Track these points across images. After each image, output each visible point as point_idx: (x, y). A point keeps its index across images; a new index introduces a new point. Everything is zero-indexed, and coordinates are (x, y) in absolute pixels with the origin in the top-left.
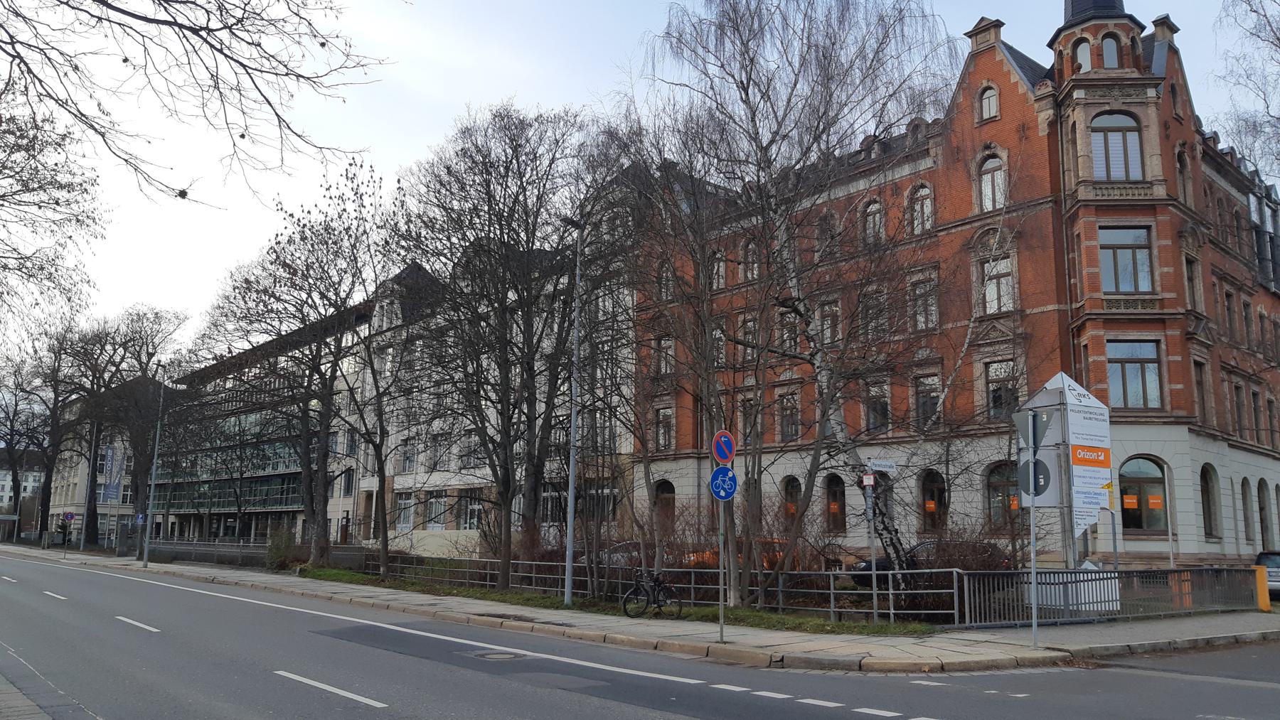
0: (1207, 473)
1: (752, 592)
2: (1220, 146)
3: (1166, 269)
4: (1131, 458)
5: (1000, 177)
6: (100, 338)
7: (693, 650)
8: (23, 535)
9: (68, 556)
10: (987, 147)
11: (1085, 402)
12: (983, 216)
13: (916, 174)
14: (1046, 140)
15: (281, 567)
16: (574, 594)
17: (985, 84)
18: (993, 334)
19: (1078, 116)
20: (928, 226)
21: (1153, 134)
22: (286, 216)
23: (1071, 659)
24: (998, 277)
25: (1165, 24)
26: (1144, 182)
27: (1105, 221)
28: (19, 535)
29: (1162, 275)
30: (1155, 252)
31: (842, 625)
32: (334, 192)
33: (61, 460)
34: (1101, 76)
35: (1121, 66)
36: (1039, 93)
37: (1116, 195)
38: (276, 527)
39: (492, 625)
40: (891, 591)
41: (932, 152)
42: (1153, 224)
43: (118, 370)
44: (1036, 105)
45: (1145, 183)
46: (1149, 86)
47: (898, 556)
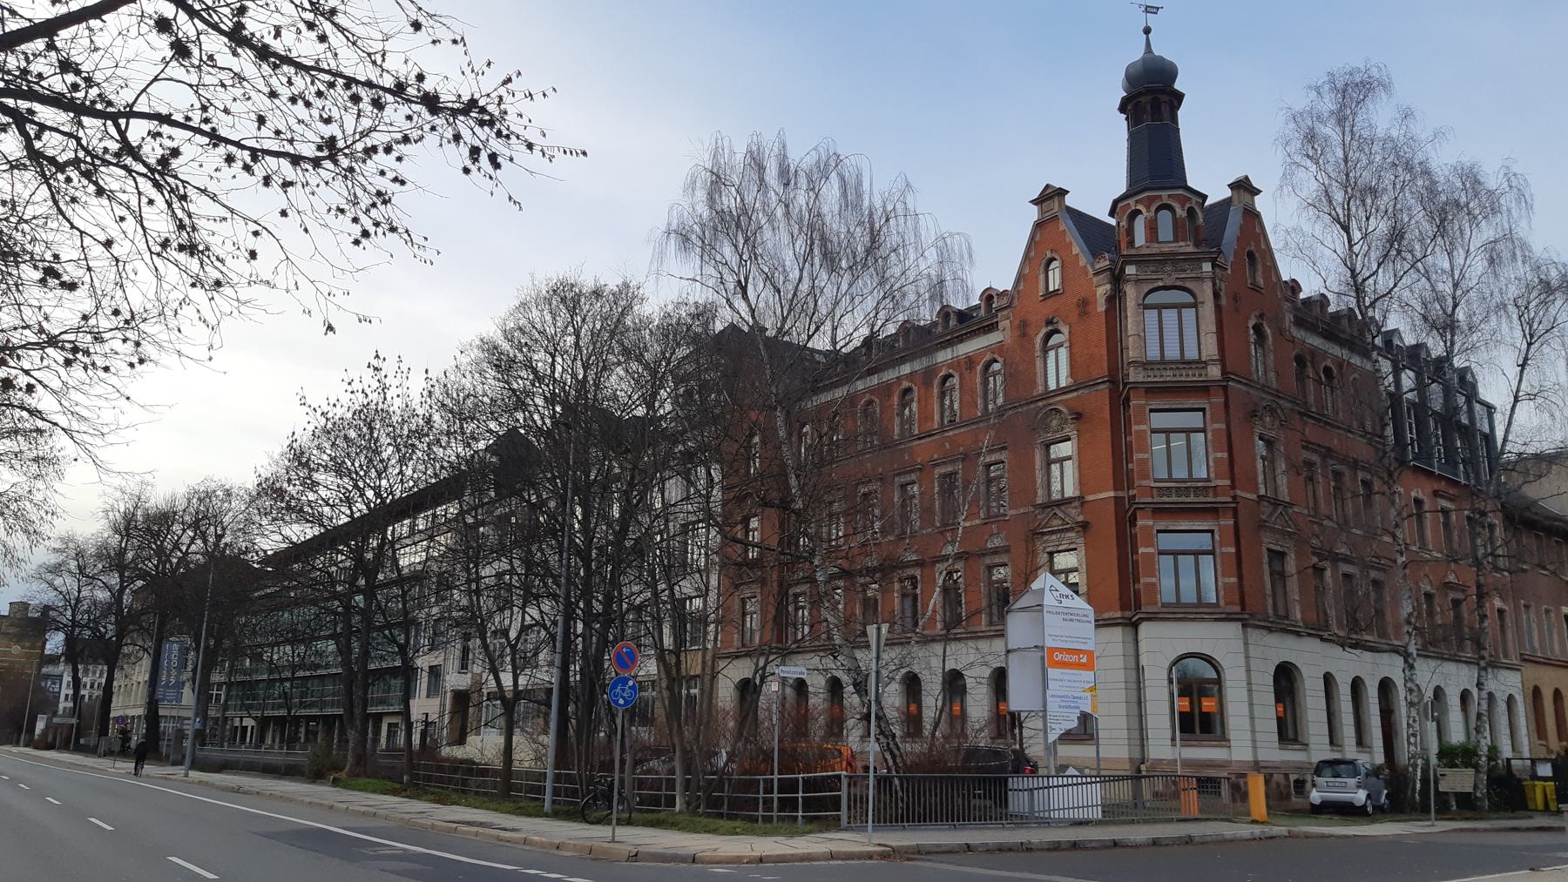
0: (1286, 678)
2: (1332, 309)
3: (1219, 455)
4: (1174, 663)
5: (1063, 352)
6: (164, 519)
8: (82, 741)
9: (119, 764)
10: (1049, 322)
12: (1048, 395)
15: (317, 776)
16: (554, 802)
17: (1049, 255)
18: (1056, 522)
19: (1131, 293)
20: (1000, 401)
21: (1208, 310)
24: (1061, 461)
25: (1243, 187)
26: (1199, 362)
27: (1155, 404)
28: (77, 741)
29: (1216, 460)
30: (1209, 436)
31: (790, 828)
32: (356, 386)
33: (125, 655)
34: (1154, 251)
35: (1176, 240)
37: (1168, 376)
39: (449, 830)
40: (762, 795)
41: (1001, 325)
42: (1207, 406)
45: (1200, 364)
46: (1205, 260)
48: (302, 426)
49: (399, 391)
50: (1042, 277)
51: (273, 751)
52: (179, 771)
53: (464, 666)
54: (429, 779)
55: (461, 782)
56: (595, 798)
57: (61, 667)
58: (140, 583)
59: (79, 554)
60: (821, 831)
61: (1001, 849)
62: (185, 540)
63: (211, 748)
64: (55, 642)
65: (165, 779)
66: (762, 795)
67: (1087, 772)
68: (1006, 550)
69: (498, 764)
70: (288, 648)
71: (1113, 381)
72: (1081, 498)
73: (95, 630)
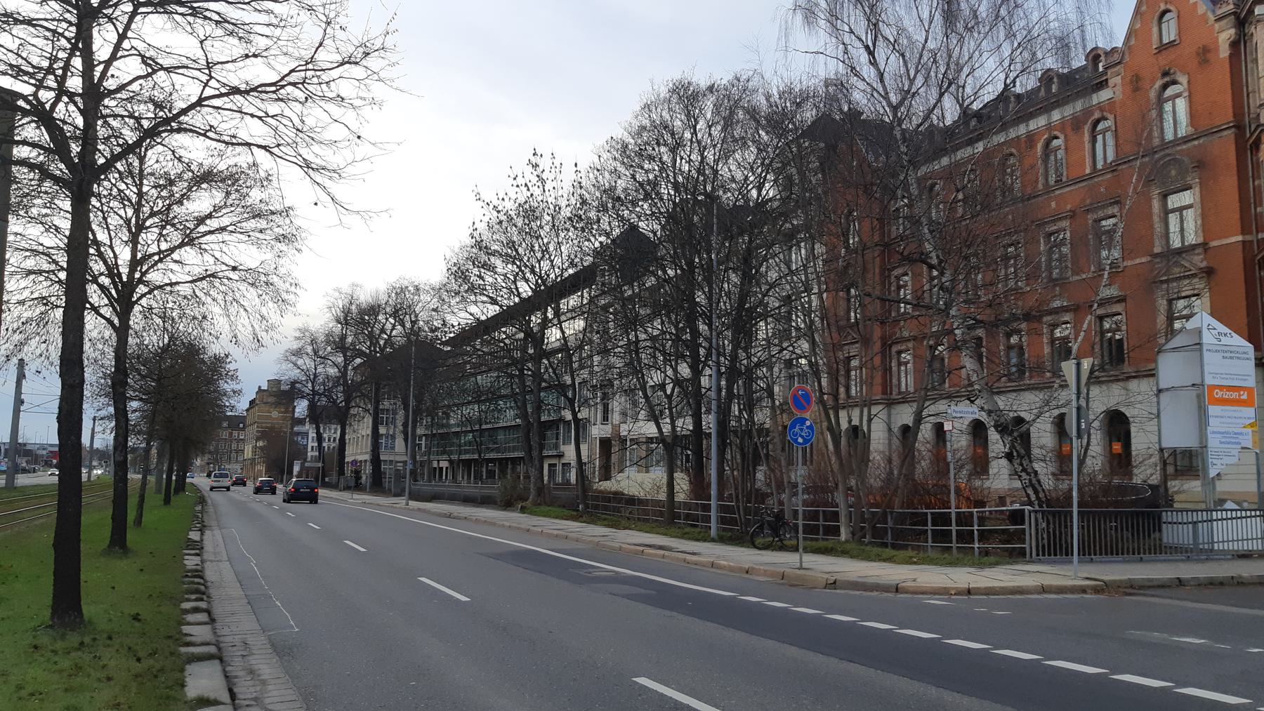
1: (863, 528)
5: (1181, 104)
6: (374, 310)
7: (773, 574)
9: (355, 496)
10: (1165, 74)
11: (1225, 340)
12: (1165, 145)
13: (1049, 127)
14: (1227, 66)
15: (507, 505)
17: (1163, 7)
18: (1176, 270)
22: (484, 205)
23: (1104, 588)
24: (1181, 210)
31: (985, 559)
32: (520, 181)
36: (1219, 12)
38: (503, 472)
39: (636, 552)
41: (1111, 83)
43: (390, 336)
44: (1217, 26)
47: (1038, 498)
48: (481, 218)
49: (554, 184)
50: (1155, 30)
51: (467, 486)
52: (401, 501)
53: (605, 418)
54: (596, 507)
55: (619, 510)
56: (761, 527)
57: (307, 426)
58: (358, 361)
59: (313, 341)
60: (1008, 563)
61: (1212, 583)
62: (388, 326)
63: (416, 483)
64: (301, 407)
65: (391, 508)
66: (976, 527)
67: (1245, 505)
68: (1121, 300)
69: (663, 496)
70: (476, 407)
71: (1239, 127)
72: (1204, 245)
73: (329, 397)
